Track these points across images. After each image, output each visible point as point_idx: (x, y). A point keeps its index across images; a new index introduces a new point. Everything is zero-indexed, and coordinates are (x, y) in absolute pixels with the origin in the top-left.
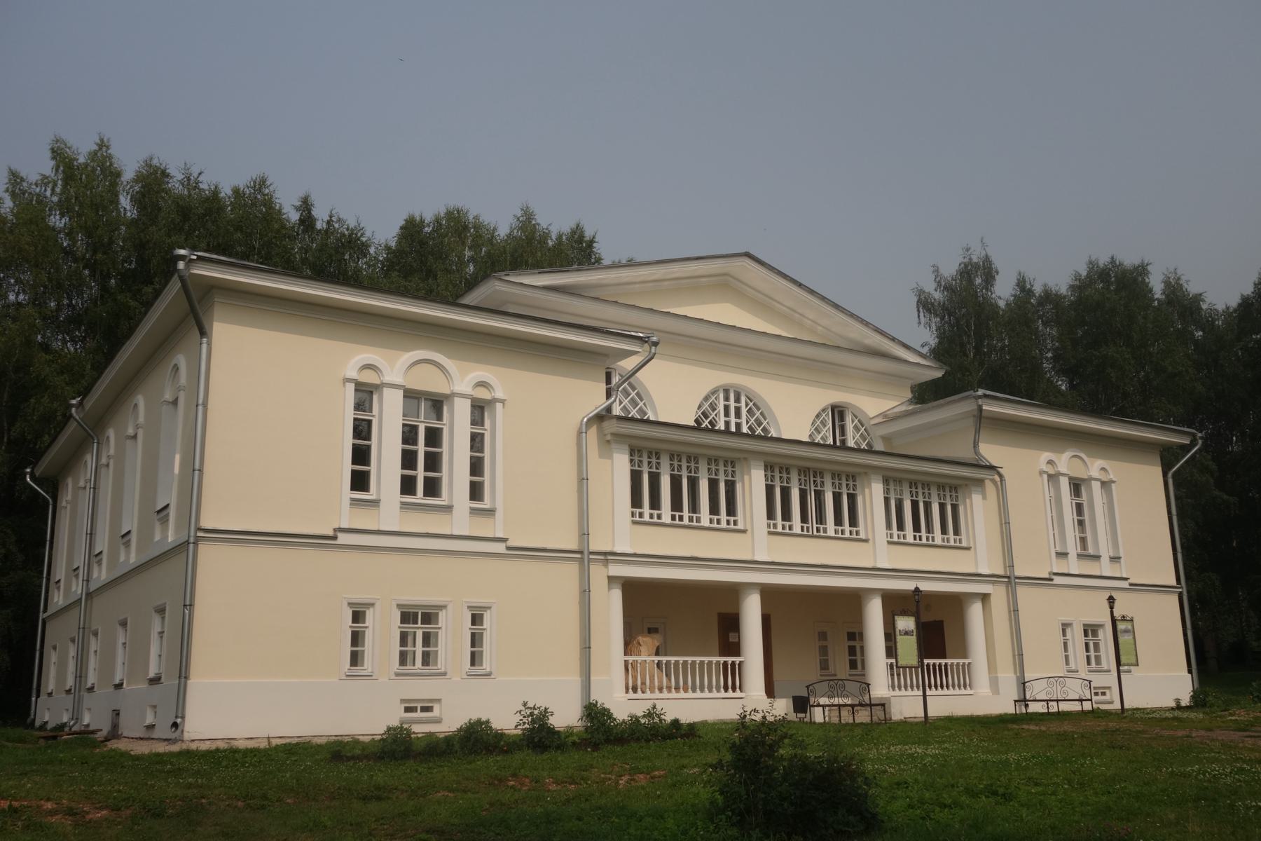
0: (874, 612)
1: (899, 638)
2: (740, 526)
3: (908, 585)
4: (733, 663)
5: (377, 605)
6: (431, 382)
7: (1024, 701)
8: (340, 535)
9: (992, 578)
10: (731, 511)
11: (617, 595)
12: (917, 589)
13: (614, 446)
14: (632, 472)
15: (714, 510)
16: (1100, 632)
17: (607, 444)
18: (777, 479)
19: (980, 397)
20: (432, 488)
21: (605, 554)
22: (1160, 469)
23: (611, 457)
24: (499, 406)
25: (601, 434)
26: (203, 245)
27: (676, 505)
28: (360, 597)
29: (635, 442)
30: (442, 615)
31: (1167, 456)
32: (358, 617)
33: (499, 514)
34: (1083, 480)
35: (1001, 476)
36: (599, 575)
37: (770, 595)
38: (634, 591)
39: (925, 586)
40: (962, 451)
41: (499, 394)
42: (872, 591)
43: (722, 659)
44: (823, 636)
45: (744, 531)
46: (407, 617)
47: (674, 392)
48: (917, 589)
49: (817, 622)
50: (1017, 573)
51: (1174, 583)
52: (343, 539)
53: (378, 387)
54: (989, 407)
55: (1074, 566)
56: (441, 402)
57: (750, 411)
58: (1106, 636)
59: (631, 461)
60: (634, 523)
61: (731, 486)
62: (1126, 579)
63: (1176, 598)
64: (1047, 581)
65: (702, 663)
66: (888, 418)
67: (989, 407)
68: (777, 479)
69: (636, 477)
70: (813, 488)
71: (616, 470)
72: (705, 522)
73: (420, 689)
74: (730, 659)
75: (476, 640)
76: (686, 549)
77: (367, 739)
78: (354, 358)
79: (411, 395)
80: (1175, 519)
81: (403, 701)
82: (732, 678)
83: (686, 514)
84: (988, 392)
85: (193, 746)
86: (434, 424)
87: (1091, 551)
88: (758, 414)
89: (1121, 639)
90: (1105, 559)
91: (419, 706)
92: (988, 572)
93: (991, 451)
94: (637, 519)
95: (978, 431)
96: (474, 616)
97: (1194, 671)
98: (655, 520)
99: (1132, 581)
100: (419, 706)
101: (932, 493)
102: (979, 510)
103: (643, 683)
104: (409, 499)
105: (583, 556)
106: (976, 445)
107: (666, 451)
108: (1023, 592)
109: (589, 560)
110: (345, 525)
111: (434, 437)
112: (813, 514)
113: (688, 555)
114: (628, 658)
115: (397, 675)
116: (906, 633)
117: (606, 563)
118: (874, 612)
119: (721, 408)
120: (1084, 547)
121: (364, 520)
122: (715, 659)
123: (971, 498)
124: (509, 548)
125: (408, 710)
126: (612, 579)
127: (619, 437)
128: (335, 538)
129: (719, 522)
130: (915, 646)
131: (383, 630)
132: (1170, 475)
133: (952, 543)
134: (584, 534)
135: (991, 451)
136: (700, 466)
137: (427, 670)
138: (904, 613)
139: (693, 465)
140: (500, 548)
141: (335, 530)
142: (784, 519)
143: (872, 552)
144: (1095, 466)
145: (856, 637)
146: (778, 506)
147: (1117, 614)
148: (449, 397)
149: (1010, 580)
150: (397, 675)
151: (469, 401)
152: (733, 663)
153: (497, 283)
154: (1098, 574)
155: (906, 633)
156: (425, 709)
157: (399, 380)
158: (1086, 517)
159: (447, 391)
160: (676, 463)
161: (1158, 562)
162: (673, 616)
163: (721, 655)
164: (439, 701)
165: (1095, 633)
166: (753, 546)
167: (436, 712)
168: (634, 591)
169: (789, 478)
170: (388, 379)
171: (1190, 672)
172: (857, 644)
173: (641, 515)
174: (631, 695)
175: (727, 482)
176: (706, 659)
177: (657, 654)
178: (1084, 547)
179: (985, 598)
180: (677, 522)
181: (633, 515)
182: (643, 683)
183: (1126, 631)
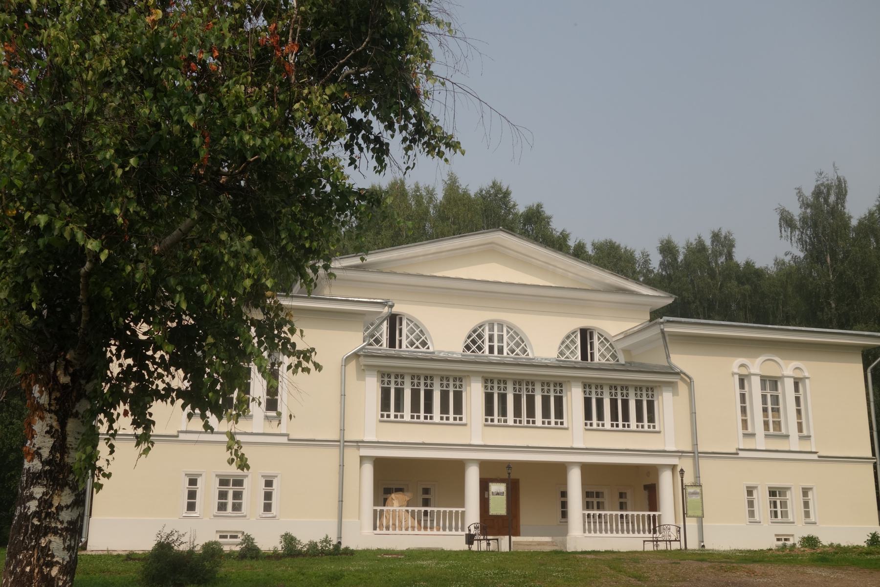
0: (473, 477)
1: (491, 497)
2: (657, 429)
4: (654, 516)
5: (814, 489)
6: (771, 371)
8: (740, 452)
9: (680, 454)
10: (651, 419)
11: (368, 470)
13: (367, 372)
14: (585, 398)
15: (639, 419)
17: (364, 370)
18: (644, 395)
19: (662, 323)
20: (777, 425)
21: (357, 442)
22: (861, 366)
23: (364, 380)
24: (807, 381)
25: (358, 365)
27: (614, 417)
28: (193, 470)
29: (485, 375)
30: (788, 493)
31: (868, 356)
32: (193, 482)
33: (812, 438)
34: (780, 378)
36: (352, 456)
37: (586, 468)
38: (382, 467)
40: (658, 360)
41: (807, 375)
45: (659, 432)
46: (772, 493)
49: (523, 486)
50: (700, 450)
51: (870, 455)
52: (182, 437)
53: (749, 376)
54: (669, 329)
56: (776, 382)
59: (486, 387)
60: (587, 430)
61: (651, 405)
62: (816, 453)
63: (871, 467)
64: (733, 455)
65: (451, 512)
67: (669, 329)
68: (644, 395)
69: (587, 402)
70: (525, 393)
71: (372, 387)
72: (510, 421)
74: (652, 513)
75: (268, 496)
77: (141, 552)
79: (764, 380)
80: (872, 404)
81: (776, 535)
83: (620, 422)
84: (671, 319)
85: (93, 553)
86: (775, 393)
89: (690, 499)
91: (229, 535)
92: (674, 449)
93: (681, 360)
94: (589, 427)
95: (666, 346)
96: (190, 480)
98: (601, 427)
99: (821, 454)
101: (626, 394)
102: (668, 405)
103: (394, 524)
105: (342, 444)
106: (668, 357)
107: (607, 384)
108: (704, 463)
109: (344, 446)
110: (741, 447)
111: (775, 399)
112: (619, 413)
113: (624, 448)
114: (376, 508)
115: (215, 516)
116: (498, 494)
117: (358, 447)
118: (473, 477)
121: (749, 444)
123: (571, 391)
124: (819, 457)
126: (362, 459)
127: (370, 367)
128: (177, 436)
129: (643, 426)
130: (505, 502)
131: (762, 499)
132: (869, 370)
134: (695, 444)
135: (681, 360)
136: (434, 382)
137: (785, 520)
139: (599, 390)
140: (284, 440)
141: (179, 432)
143: (575, 438)
144: (787, 367)
148: (782, 378)
149: (695, 455)
150: (215, 516)
152: (654, 516)
154: (787, 449)
155: (498, 494)
157: (757, 371)
158: (748, 404)
159: (780, 375)
160: (613, 391)
163: (650, 510)
164: (793, 535)
166: (472, 434)
168: (382, 467)
169: (403, 382)
170: (752, 371)
173: (591, 425)
174: (587, 534)
175: (648, 401)
176: (641, 513)
177: (407, 506)
179: (673, 467)
180: (518, 424)
181: (586, 425)
182: (394, 524)
183: (695, 493)
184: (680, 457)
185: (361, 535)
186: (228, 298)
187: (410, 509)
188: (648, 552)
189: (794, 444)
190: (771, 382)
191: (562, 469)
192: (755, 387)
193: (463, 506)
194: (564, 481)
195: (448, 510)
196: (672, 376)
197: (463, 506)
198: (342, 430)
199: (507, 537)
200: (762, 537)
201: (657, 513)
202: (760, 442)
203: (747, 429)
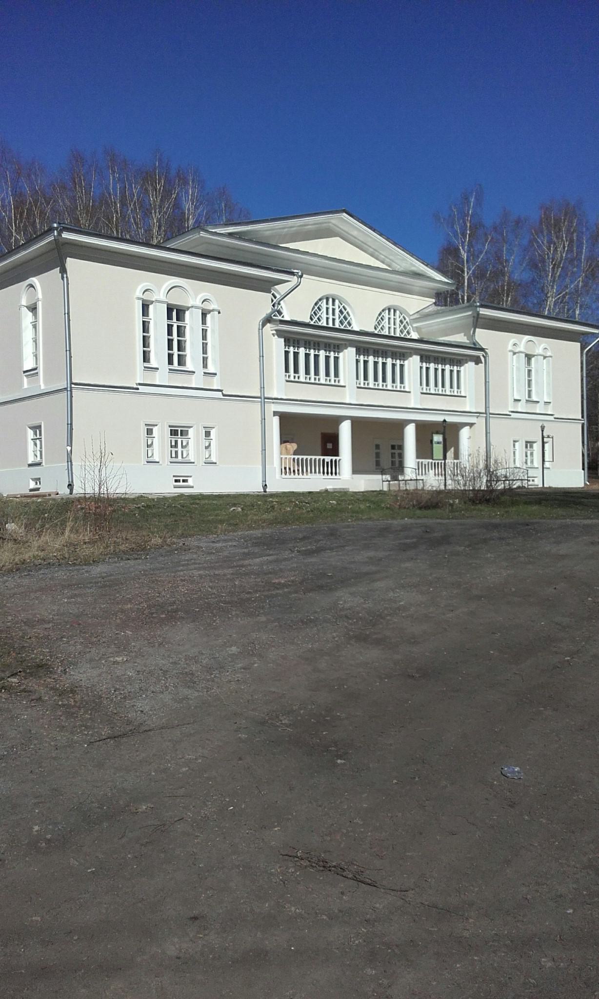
0: (410, 432)
1: (434, 445)
3: (440, 418)
4: (302, 459)
7: (265, 491)
12: (445, 421)
16: (535, 445)
20: (181, 361)
26: (508, 301)
29: (286, 335)
30: (191, 431)
35: (486, 353)
37: (358, 424)
38: (286, 420)
39: (450, 419)
42: (409, 422)
43: (322, 458)
44: (377, 447)
46: (174, 433)
47: (300, 301)
48: (445, 421)
55: (520, 407)
56: (184, 312)
57: (341, 312)
58: (537, 447)
66: (424, 316)
73: (182, 470)
76: (312, 397)
78: (142, 282)
82: (332, 469)
87: (534, 398)
88: (345, 313)
90: (542, 403)
96: (152, 433)
97: (586, 469)
100: (181, 479)
104: (171, 367)
105: (264, 399)
111: (181, 332)
116: (438, 443)
118: (410, 432)
119: (324, 310)
120: (529, 396)
122: (318, 457)
125: (176, 481)
133: (381, 387)
135: (483, 336)
138: (437, 433)
142: (315, 374)
144: (194, 294)
145: (398, 449)
146: (290, 365)
147: (545, 434)
151: (200, 311)
153: (202, 234)
155: (438, 443)
156: (184, 481)
161: (573, 405)
162: (310, 435)
165: (531, 447)
167: (190, 482)
168: (286, 420)
171: (583, 469)
172: (397, 452)
177: (295, 454)
178: (529, 396)
179: (471, 425)
184: (478, 417)
185: (280, 484)
186: (56, 229)
187: (296, 457)
188: (450, 491)
189: (196, 381)
190: (176, 312)
191: (399, 426)
192: (158, 317)
193: (338, 455)
194: (401, 436)
195: (309, 457)
196: (475, 354)
197: (338, 455)
198: (262, 388)
199: (78, 490)
200: (158, 483)
201: (338, 458)
202: (162, 376)
203: (148, 361)
